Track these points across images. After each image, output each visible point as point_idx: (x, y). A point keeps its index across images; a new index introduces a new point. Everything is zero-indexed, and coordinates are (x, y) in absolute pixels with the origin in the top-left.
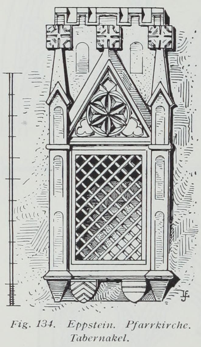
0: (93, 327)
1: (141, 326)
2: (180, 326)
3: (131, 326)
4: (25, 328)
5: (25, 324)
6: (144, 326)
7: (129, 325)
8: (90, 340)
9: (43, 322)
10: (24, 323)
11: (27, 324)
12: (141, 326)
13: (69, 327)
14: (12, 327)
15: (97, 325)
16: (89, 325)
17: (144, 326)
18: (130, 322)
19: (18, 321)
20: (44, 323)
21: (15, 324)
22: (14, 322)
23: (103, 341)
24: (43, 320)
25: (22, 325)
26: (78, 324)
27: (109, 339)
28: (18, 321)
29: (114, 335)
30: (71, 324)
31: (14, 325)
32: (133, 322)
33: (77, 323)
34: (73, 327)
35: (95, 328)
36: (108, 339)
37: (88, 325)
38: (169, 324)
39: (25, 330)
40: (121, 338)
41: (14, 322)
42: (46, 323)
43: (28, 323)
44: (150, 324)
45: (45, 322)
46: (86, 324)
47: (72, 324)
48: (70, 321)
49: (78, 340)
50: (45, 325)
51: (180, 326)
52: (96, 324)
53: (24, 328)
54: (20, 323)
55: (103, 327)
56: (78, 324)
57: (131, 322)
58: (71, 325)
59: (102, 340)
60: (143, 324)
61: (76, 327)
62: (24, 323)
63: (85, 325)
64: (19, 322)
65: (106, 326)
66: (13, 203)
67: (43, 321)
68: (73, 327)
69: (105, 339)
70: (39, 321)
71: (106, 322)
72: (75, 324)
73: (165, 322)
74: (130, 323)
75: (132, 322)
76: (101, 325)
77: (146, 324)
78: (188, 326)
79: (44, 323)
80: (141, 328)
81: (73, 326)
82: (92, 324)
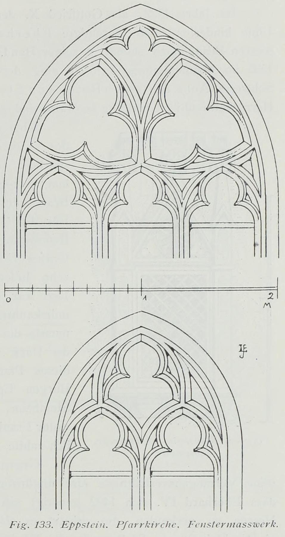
0: (212, 526)
1: (130, 526)
2: (233, 525)
3: (121, 526)
4: (24, 529)
5: (24, 525)
6: (134, 526)
7: (119, 525)
8: (217, 526)
9: (41, 523)
10: (22, 524)
11: (26, 525)
12: (130, 526)
13: (63, 527)
14: (11, 527)
15: (215, 525)
16: (249, 524)
17: (134, 526)
18: (120, 522)
19: (17, 522)
20: (41, 524)
21: (193, 524)
22: (13, 522)
23: (233, 527)
24: (41, 521)
25: (20, 526)
26: (71, 524)
27: (240, 525)
28: (17, 522)
29: (147, 522)
30: (64, 525)
31: (191, 525)
32: (123, 522)
33: (71, 523)
34: (67, 527)
35: (266, 522)
36: (238, 526)
37: (81, 525)
38: (268, 523)
39: (23, 531)
40: (263, 524)
41: (64, 522)
42: (44, 524)
43: (26, 524)
44: (265, 523)
45: (43, 523)
46: (73, 524)
47: (66, 524)
48: (63, 522)
49: (238, 526)
50: (49, 526)
51: (168, 525)
52: (214, 524)
53: (23, 528)
54: (19, 524)
55: (152, 527)
56: (71, 524)
57: (121, 523)
58: (65, 526)
59: (232, 526)
60: (240, 524)
61: (69, 528)
62: (22, 524)
63: (73, 524)
64: (18, 523)
65: (99, 525)
66: (39, 164)
67: (47, 522)
68: (67, 527)
69: (235, 525)
70: (38, 523)
71: (154, 522)
72: (69, 525)
73: (154, 522)
74: (120, 523)
75: (122, 523)
76: (219, 525)
77: (141, 524)
78: (177, 526)
79: (41, 524)
80: (239, 527)
81: (66, 527)
82: (210, 523)
